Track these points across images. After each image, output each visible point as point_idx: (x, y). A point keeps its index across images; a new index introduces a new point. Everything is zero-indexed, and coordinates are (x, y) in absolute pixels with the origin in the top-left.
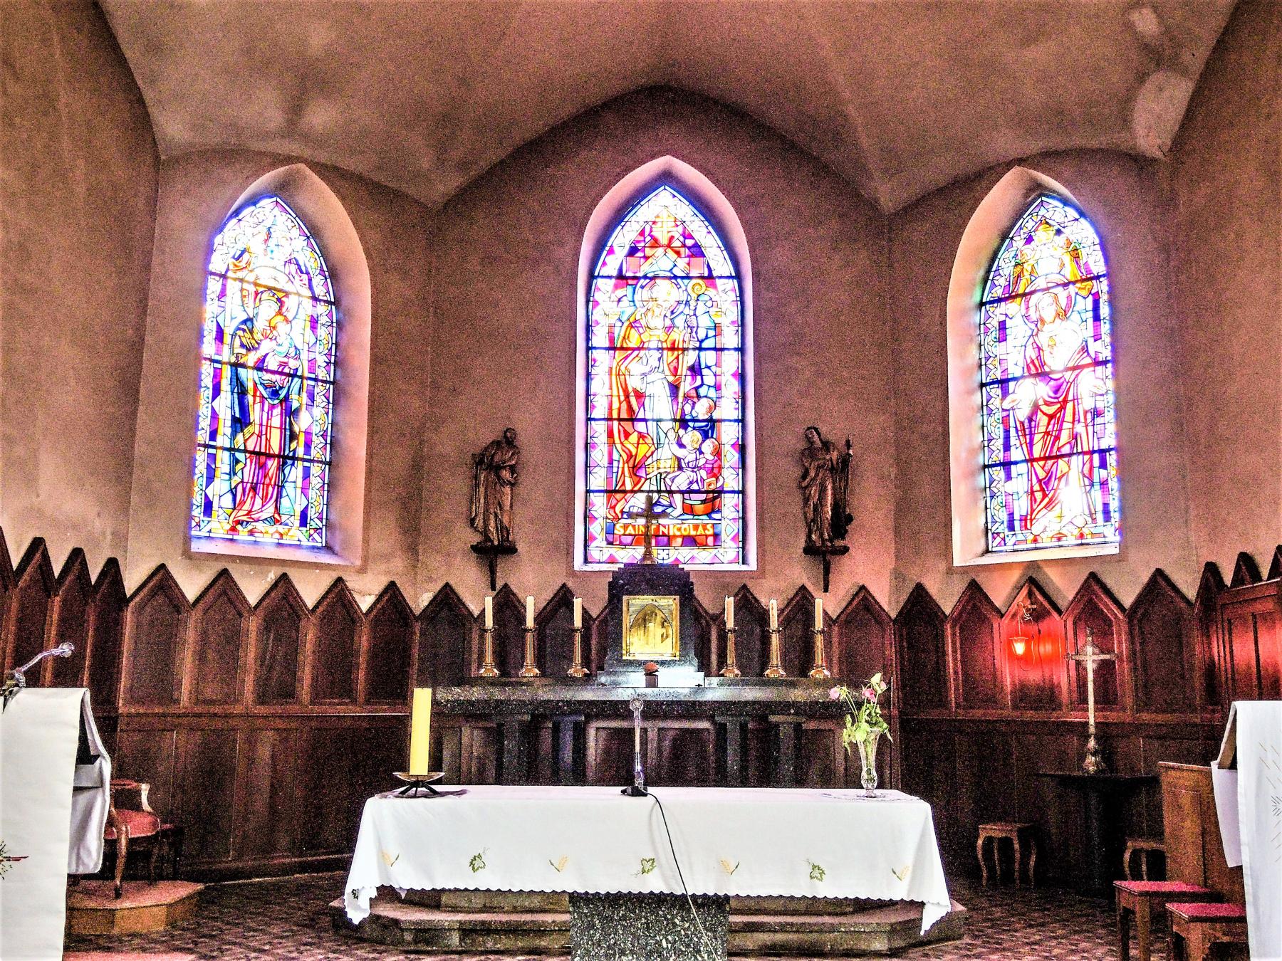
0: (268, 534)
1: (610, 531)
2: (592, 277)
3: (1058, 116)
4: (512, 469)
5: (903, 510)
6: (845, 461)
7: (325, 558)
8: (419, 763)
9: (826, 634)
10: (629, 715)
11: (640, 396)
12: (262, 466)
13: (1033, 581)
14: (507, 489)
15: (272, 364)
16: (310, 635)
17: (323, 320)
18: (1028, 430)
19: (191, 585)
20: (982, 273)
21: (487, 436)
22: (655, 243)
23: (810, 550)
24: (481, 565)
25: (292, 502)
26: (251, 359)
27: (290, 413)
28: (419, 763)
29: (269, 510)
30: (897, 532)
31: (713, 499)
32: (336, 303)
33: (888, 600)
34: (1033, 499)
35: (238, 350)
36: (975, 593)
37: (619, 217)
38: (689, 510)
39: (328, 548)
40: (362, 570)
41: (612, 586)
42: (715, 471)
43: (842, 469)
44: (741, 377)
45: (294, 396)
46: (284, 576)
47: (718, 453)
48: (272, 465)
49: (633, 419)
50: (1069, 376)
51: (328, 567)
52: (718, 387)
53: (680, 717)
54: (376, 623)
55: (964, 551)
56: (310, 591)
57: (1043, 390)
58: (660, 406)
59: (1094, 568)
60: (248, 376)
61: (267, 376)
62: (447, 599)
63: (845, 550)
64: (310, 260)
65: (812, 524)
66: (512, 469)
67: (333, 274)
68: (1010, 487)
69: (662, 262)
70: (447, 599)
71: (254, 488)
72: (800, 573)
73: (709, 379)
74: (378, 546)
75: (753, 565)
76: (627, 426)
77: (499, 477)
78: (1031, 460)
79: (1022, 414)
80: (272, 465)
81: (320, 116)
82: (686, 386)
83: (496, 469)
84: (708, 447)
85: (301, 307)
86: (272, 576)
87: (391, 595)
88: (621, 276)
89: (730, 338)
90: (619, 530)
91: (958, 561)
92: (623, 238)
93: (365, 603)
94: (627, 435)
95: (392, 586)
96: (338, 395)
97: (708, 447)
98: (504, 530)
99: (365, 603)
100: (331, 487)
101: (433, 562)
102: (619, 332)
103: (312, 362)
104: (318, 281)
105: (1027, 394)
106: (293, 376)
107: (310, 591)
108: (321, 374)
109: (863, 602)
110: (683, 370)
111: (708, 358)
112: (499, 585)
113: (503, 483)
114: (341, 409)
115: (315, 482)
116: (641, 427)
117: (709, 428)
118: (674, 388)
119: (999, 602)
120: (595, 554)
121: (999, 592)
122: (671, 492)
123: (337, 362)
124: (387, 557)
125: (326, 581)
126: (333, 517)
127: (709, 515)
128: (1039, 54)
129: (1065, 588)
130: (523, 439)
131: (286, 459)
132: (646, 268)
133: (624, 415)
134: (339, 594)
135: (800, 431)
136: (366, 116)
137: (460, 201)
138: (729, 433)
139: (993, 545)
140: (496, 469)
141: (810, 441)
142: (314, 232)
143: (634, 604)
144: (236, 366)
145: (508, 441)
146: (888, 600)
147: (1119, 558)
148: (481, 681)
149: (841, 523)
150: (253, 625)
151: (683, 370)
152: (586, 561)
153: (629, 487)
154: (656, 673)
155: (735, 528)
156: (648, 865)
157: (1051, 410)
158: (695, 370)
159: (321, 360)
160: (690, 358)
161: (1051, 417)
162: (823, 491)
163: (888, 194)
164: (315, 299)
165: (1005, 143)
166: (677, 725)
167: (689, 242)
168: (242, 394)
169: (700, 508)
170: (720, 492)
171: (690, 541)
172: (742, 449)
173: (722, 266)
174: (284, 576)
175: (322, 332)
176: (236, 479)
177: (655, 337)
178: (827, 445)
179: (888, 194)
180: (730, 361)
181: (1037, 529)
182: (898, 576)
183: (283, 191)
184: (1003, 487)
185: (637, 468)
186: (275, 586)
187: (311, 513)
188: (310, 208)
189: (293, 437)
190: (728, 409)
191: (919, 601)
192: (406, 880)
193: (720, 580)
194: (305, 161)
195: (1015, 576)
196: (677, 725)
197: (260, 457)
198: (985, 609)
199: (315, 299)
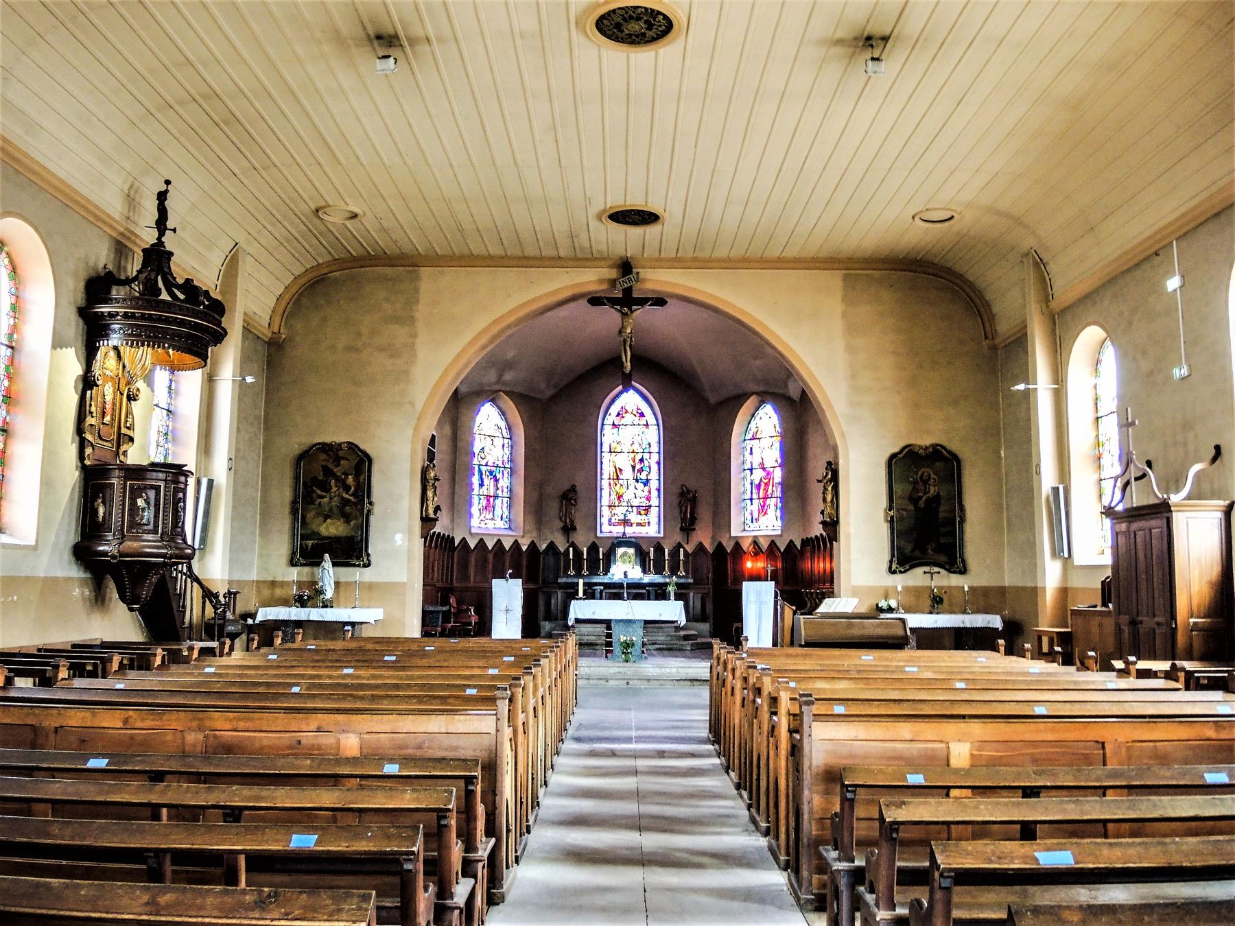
0: (490, 524)
1: (610, 520)
2: (603, 425)
3: (767, 382)
4: (575, 500)
5: (715, 515)
6: (695, 497)
7: (510, 533)
8: (581, 594)
9: (685, 563)
10: (623, 587)
11: (621, 470)
12: (488, 500)
13: (755, 543)
14: (573, 507)
15: (490, 463)
16: (473, 559)
17: (506, 445)
18: (758, 487)
19: (472, 544)
20: (745, 429)
21: (567, 486)
22: (627, 412)
23: (682, 529)
24: (564, 535)
25: (498, 512)
26: (483, 462)
27: (496, 480)
28: (581, 594)
29: (491, 516)
30: (713, 523)
31: (647, 509)
32: (510, 439)
33: (709, 547)
34: (759, 512)
35: (480, 459)
36: (737, 546)
37: (613, 401)
38: (639, 513)
39: (510, 528)
40: (523, 537)
41: (613, 544)
42: (648, 499)
43: (694, 501)
44: (658, 463)
45: (497, 475)
46: (499, 540)
47: (650, 492)
48: (492, 499)
49: (618, 479)
50: (771, 470)
51: (511, 536)
52: (650, 468)
53: (634, 588)
54: (512, 555)
55: (735, 532)
56: (507, 545)
57: (762, 474)
58: (628, 474)
59: (773, 538)
60: (484, 469)
61: (489, 468)
62: (552, 546)
63: (694, 529)
64: (503, 424)
65: (683, 520)
66: (575, 500)
67: (509, 428)
68: (752, 508)
69: (628, 418)
70: (552, 546)
71: (486, 508)
72: (678, 537)
73: (646, 464)
74: (528, 528)
75: (662, 535)
76: (616, 481)
77: (571, 502)
78: (759, 498)
79: (757, 482)
80: (492, 499)
81: (508, 376)
82: (638, 467)
83: (569, 500)
84: (646, 489)
85: (499, 442)
86: (495, 540)
87: (533, 545)
88: (614, 424)
89: (655, 448)
90: (613, 521)
91: (732, 535)
92: (614, 409)
93: (524, 548)
94: (616, 485)
95: (533, 542)
96: (512, 472)
97: (646, 489)
98: (572, 522)
99: (524, 548)
100: (510, 506)
101: (546, 532)
102: (613, 445)
103: (503, 461)
104: (504, 431)
105: (758, 475)
106: (497, 467)
107: (507, 545)
108: (507, 466)
109: (700, 547)
110: (637, 461)
111: (646, 456)
112: (571, 541)
113: (572, 505)
114: (513, 478)
115: (505, 505)
116: (621, 481)
117: (646, 482)
118: (634, 467)
119: (745, 549)
120: (603, 530)
121: (746, 545)
122: (632, 507)
123: (511, 460)
124: (530, 532)
125: (512, 541)
126: (511, 517)
127: (646, 515)
128: (758, 362)
129: (764, 545)
130: (578, 489)
131: (496, 497)
132: (623, 421)
133: (615, 477)
134: (516, 544)
135: (679, 486)
136: (522, 375)
137: (554, 399)
138: (654, 484)
139: (746, 528)
140: (569, 500)
141: (682, 489)
142: (503, 413)
143: (620, 551)
144: (479, 465)
145: (573, 489)
146: (709, 547)
147: (781, 536)
148: (570, 576)
149: (693, 520)
150: (491, 557)
151: (637, 461)
152: (601, 532)
153: (617, 504)
154: (1103, 511)
155: (656, 520)
156: (628, 614)
157: (766, 481)
158: (642, 460)
159: (506, 460)
160: (639, 457)
161: (766, 484)
162: (687, 508)
163: (713, 399)
164: (503, 438)
165: (752, 387)
166: (634, 591)
167: (639, 411)
168: (481, 475)
169: (643, 512)
170: (650, 506)
171: (639, 524)
172: (659, 490)
173: (652, 421)
174: (499, 540)
175: (506, 449)
176: (481, 505)
177: (626, 448)
178: (688, 491)
179: (713, 399)
180: (655, 457)
181: (760, 523)
182: (713, 538)
183: (493, 401)
184: (749, 507)
185: (620, 497)
186: (496, 544)
187: (504, 516)
188: (502, 406)
189: (498, 489)
190: (654, 476)
191: (720, 547)
192: (581, 616)
193: (649, 539)
194: (503, 391)
195: (750, 540)
196: (634, 591)
197: (488, 497)
198: (741, 552)
199: (503, 438)
